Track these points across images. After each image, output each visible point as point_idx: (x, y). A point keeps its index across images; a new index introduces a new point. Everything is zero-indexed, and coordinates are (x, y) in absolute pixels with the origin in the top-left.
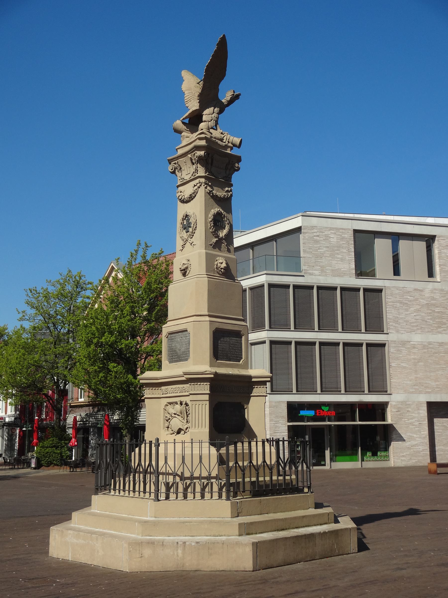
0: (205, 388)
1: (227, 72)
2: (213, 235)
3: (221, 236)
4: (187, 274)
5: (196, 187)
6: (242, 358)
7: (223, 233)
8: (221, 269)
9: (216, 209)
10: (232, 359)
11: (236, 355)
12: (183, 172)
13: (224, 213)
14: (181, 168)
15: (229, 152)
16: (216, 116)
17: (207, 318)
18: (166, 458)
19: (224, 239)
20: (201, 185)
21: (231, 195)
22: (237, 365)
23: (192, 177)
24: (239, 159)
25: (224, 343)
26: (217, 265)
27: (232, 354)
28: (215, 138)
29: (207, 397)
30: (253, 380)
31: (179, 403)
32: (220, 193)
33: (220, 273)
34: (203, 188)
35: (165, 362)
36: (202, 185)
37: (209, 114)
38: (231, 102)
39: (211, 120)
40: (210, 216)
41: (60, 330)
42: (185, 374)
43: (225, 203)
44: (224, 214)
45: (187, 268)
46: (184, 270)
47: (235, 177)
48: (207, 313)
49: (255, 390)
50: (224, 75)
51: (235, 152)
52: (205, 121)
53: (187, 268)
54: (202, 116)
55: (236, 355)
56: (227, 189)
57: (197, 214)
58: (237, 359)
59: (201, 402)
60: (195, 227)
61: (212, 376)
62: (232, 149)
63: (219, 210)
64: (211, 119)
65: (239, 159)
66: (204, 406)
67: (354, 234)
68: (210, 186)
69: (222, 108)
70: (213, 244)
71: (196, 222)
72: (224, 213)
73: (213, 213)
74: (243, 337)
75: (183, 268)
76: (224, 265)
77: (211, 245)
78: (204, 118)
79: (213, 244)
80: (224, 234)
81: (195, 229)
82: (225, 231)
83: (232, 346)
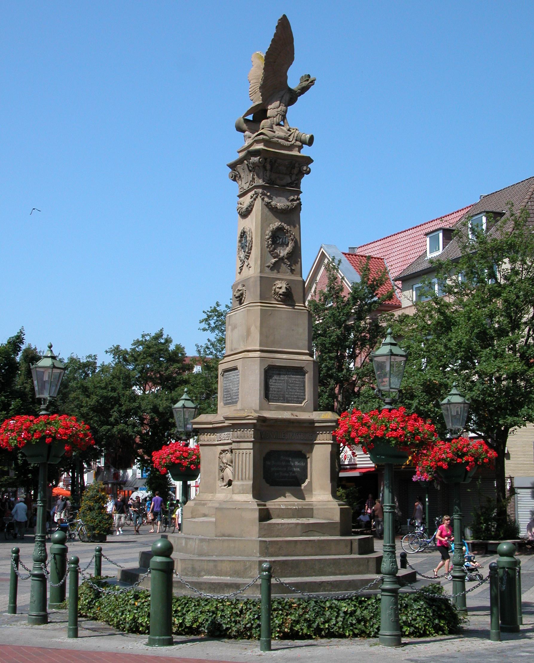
0: (250, 434)
1: (295, 56)
2: (272, 255)
3: (282, 255)
4: (242, 301)
5: (253, 199)
6: (304, 399)
7: (283, 252)
8: (280, 294)
9: (277, 224)
10: (291, 400)
11: (296, 395)
12: (243, 180)
13: (286, 227)
14: (240, 176)
15: (298, 154)
16: (283, 110)
17: (258, 354)
18: (323, 505)
19: (286, 258)
20: (257, 197)
21: (300, 204)
22: (298, 407)
23: (250, 187)
24: (309, 160)
25: (278, 383)
26: (275, 290)
27: (292, 395)
28: (278, 137)
29: (250, 445)
30: (316, 425)
31: (230, 451)
32: (280, 203)
33: (279, 299)
34: (259, 200)
35: (220, 404)
36: (259, 197)
37: (273, 109)
38: (304, 90)
39: (277, 115)
40: (267, 232)
41: (287, 385)
42: (226, 420)
43: (291, 215)
44: (286, 228)
45: (242, 294)
46: (239, 297)
47: (305, 182)
48: (258, 348)
49: (319, 437)
50: (292, 59)
51: (306, 151)
52: (270, 117)
53: (242, 294)
54: (266, 111)
55: (296, 395)
56: (292, 197)
57: (253, 230)
58: (294, 401)
59: (244, 451)
60: (250, 246)
61: (255, 421)
62: (300, 148)
63: (280, 224)
64: (276, 113)
65: (309, 160)
66: (248, 455)
67: (260, 281)
68: (268, 196)
69: (292, 97)
70: (271, 265)
71: (251, 241)
72: (286, 227)
73: (272, 228)
74: (307, 375)
75: (237, 295)
76: (283, 290)
77: (268, 267)
78: (269, 113)
79: (271, 265)
80: (286, 252)
81: (251, 249)
82: (288, 249)
83: (291, 385)
